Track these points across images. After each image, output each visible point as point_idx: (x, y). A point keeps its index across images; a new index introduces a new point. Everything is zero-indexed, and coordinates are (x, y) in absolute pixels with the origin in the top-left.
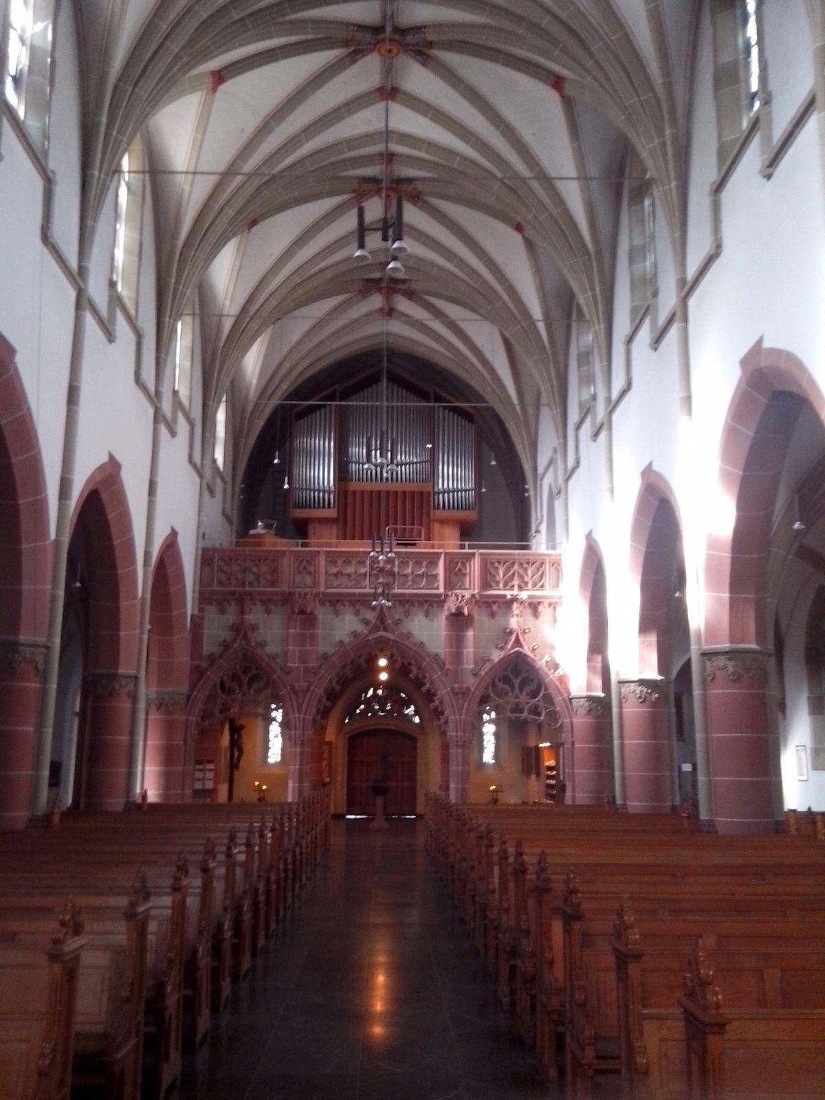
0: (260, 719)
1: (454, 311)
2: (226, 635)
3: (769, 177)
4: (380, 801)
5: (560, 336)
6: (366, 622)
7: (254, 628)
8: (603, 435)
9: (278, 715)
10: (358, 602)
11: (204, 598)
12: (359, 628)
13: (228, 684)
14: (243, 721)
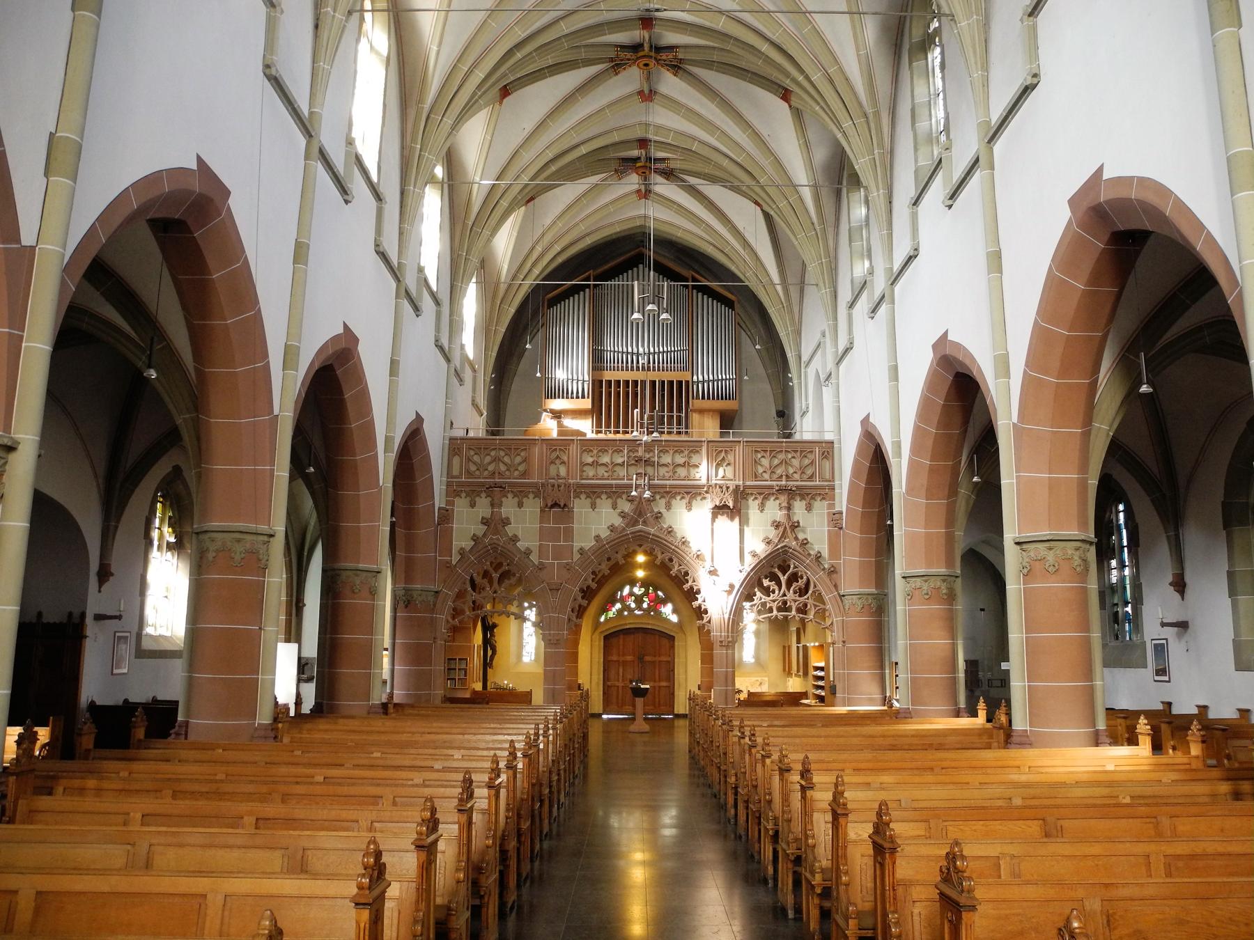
0: (512, 617)
1: (715, 192)
2: (480, 530)
3: (950, 207)
4: (639, 701)
5: (830, 217)
6: (623, 515)
7: (506, 522)
8: (884, 308)
9: (531, 614)
10: (616, 492)
11: (453, 490)
12: (618, 522)
13: (478, 580)
14: (496, 620)
